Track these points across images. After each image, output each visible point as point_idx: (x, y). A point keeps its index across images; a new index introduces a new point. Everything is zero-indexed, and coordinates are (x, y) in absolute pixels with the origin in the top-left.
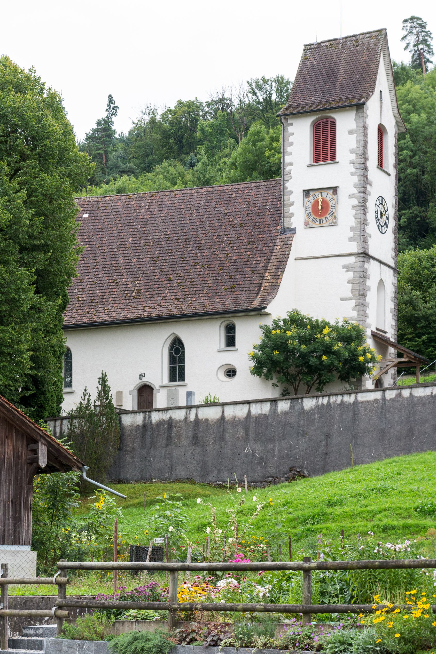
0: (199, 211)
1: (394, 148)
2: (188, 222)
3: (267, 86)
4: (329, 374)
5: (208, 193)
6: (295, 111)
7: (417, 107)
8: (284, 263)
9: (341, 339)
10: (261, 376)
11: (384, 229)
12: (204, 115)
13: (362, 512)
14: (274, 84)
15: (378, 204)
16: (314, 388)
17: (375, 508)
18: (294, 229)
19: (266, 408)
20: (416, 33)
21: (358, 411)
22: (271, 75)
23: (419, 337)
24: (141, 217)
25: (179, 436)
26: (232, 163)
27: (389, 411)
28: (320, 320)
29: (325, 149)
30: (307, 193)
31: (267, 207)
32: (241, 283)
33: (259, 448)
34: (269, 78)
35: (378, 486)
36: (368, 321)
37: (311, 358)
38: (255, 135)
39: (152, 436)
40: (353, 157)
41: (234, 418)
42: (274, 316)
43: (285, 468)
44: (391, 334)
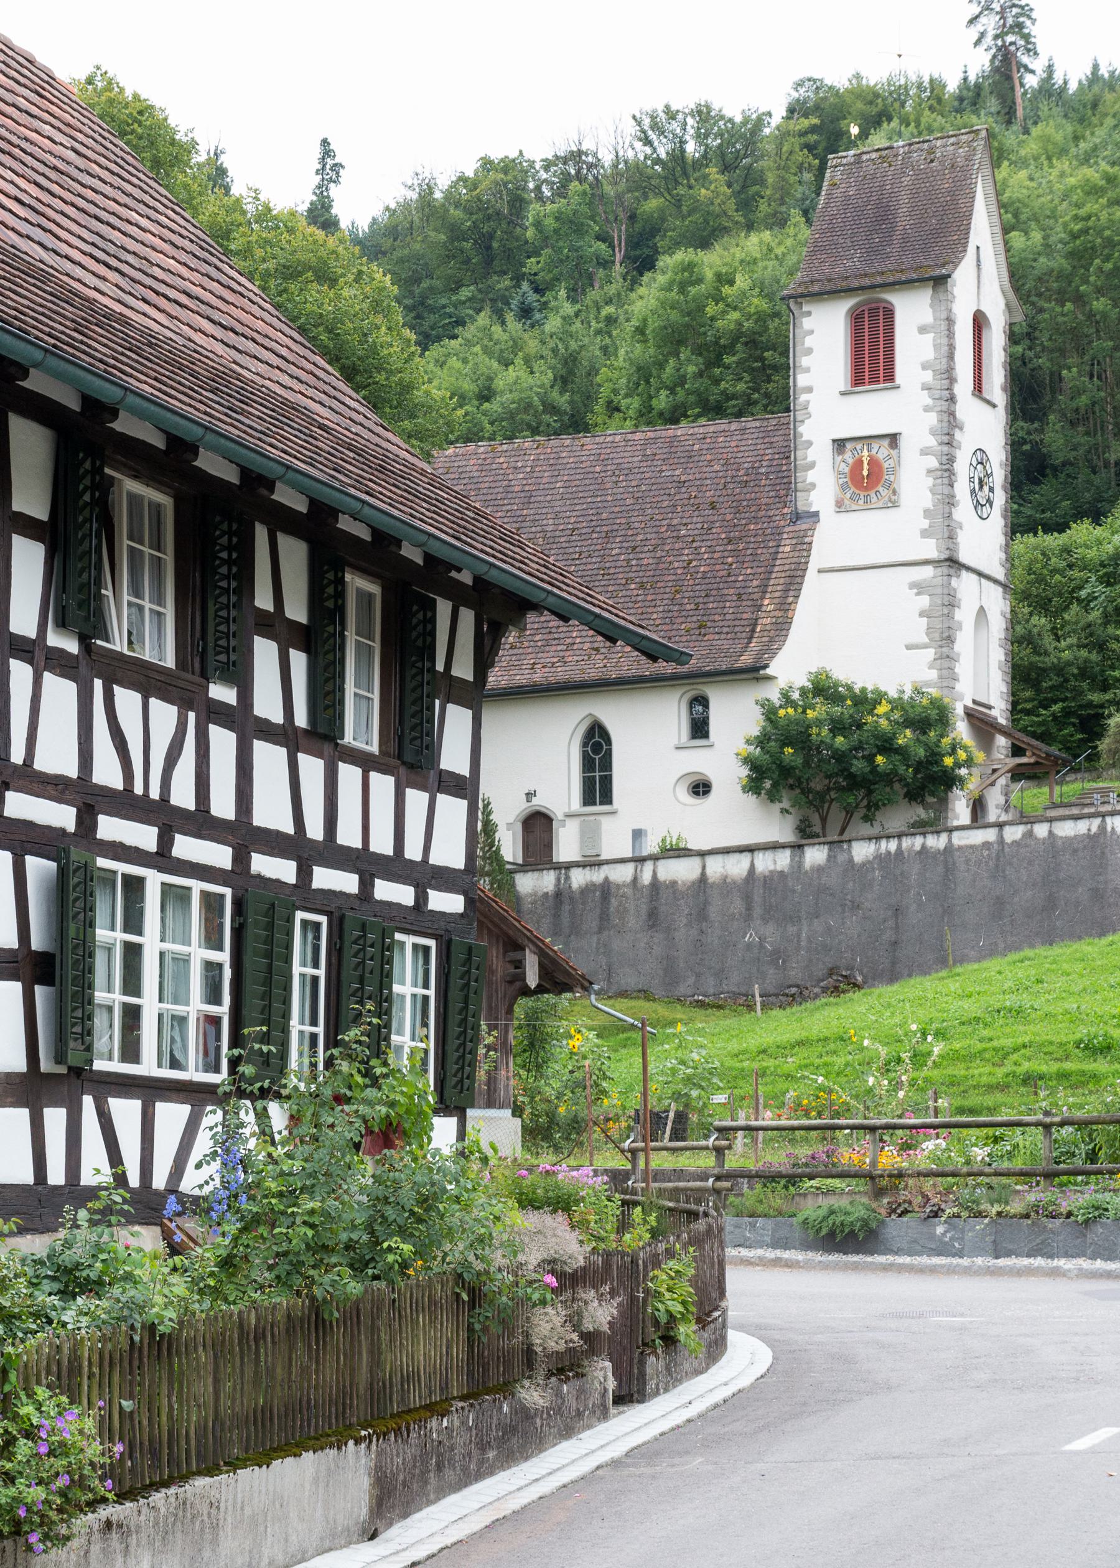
0: (631, 477)
1: (1003, 353)
2: (609, 498)
3: (675, 126)
4: (888, 789)
5: (647, 442)
6: (816, 288)
7: (1023, 217)
8: (798, 580)
9: (909, 723)
10: (759, 794)
11: (986, 510)
12: (538, 188)
13: (985, 1050)
14: (690, 121)
15: (974, 463)
16: (857, 815)
17: (1007, 1043)
18: (816, 514)
19: (783, 860)
20: (998, 9)
21: (954, 863)
22: (684, 102)
23: (1045, 708)
24: (517, 489)
25: (622, 912)
26: (637, 328)
27: (1011, 864)
28: (870, 688)
29: (874, 362)
30: (840, 444)
31: (763, 470)
32: (717, 618)
33: (771, 934)
34: (680, 108)
35: (1008, 1004)
36: (959, 687)
37: (855, 762)
38: (684, 270)
39: (572, 913)
40: (928, 376)
41: (725, 878)
42: (782, 683)
43: (820, 970)
44: (1000, 712)
